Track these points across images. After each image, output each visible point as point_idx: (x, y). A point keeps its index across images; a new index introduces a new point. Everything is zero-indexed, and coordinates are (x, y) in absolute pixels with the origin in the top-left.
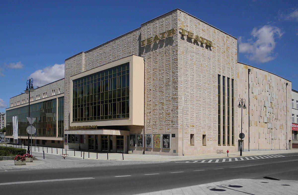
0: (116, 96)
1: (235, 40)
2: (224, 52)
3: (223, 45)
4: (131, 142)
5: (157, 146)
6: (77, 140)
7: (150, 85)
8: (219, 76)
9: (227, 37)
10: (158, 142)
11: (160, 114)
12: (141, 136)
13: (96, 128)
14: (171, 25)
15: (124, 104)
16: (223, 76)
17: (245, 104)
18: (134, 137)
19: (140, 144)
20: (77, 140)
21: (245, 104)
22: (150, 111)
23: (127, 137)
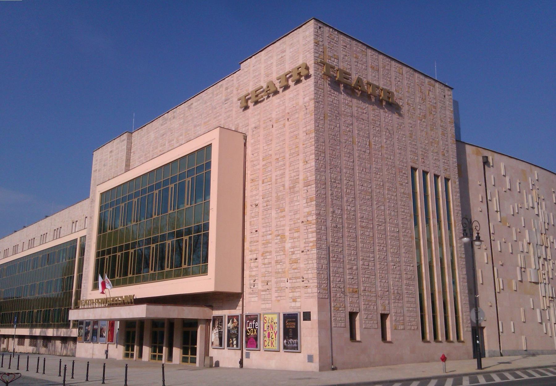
0: (454, 197)
1: (449, 90)
2: (425, 116)
3: (422, 102)
4: (213, 335)
5: (270, 344)
6: (102, 336)
7: (256, 195)
8: (414, 170)
9: (430, 84)
10: (271, 334)
11: (277, 262)
12: (235, 321)
13: (131, 303)
14: (301, 56)
15: (197, 238)
16: (423, 171)
17: (478, 234)
18: (222, 322)
19: (232, 340)
20: (102, 336)
21: (478, 234)
22: (255, 256)
23: (348, 317)
